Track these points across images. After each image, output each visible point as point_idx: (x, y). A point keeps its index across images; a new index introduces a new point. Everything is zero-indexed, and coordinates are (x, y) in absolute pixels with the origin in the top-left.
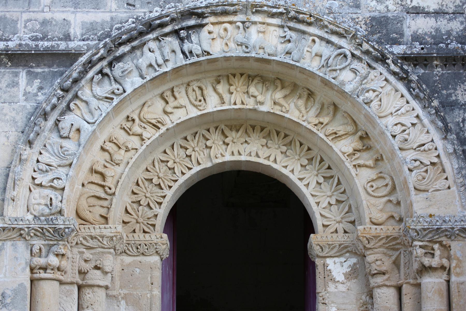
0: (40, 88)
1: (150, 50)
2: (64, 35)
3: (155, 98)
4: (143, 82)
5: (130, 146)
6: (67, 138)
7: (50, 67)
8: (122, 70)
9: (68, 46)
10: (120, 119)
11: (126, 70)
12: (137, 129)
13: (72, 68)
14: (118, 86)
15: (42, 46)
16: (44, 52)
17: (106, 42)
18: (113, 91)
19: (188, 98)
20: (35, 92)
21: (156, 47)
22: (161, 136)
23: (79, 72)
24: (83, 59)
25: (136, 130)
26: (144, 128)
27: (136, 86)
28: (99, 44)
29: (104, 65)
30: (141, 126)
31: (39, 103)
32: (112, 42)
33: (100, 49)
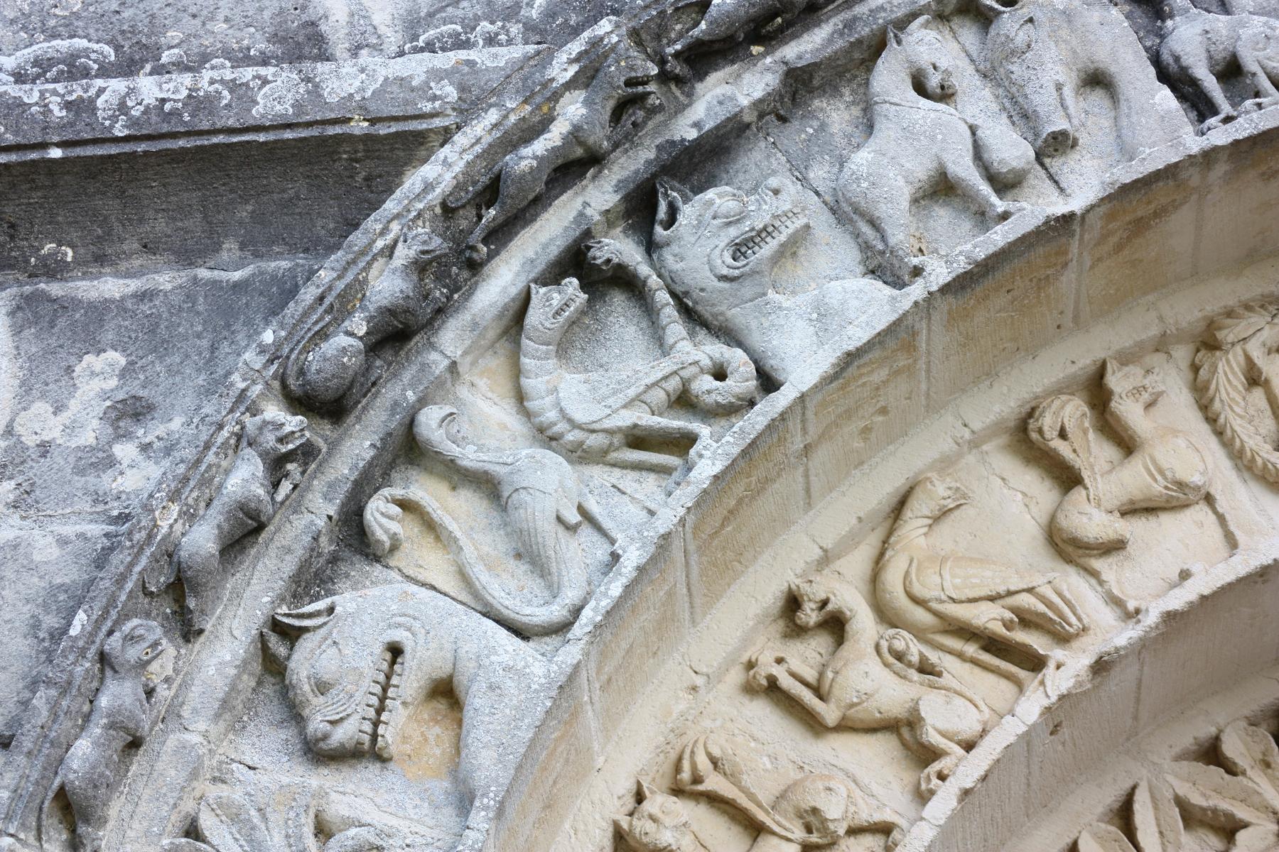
0: (130, 412)
1: (920, 87)
2: (274, 38)
3: (971, 459)
4: (906, 304)
5: (833, 809)
6: (368, 753)
7: (187, 256)
8: (733, 232)
9: (316, 92)
10: (735, 623)
11: (765, 232)
12: (867, 679)
13: (357, 239)
14: (713, 350)
15: (123, 108)
16: (141, 147)
17: (596, 43)
18: (686, 383)
19: (1219, 434)
20: (87, 438)
21: (964, 63)
22: (1057, 718)
23: (420, 267)
24: (440, 172)
25: (866, 685)
26: (925, 668)
27: (858, 335)
28: (544, 59)
29: (594, 214)
30: (899, 657)
31: (123, 518)
32: (640, 44)
33: (556, 96)
